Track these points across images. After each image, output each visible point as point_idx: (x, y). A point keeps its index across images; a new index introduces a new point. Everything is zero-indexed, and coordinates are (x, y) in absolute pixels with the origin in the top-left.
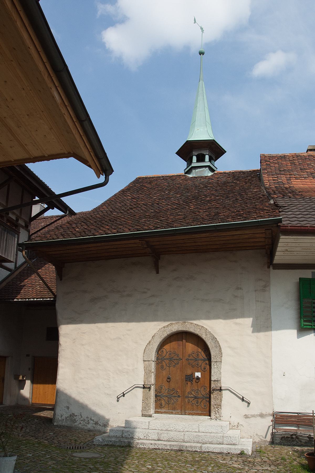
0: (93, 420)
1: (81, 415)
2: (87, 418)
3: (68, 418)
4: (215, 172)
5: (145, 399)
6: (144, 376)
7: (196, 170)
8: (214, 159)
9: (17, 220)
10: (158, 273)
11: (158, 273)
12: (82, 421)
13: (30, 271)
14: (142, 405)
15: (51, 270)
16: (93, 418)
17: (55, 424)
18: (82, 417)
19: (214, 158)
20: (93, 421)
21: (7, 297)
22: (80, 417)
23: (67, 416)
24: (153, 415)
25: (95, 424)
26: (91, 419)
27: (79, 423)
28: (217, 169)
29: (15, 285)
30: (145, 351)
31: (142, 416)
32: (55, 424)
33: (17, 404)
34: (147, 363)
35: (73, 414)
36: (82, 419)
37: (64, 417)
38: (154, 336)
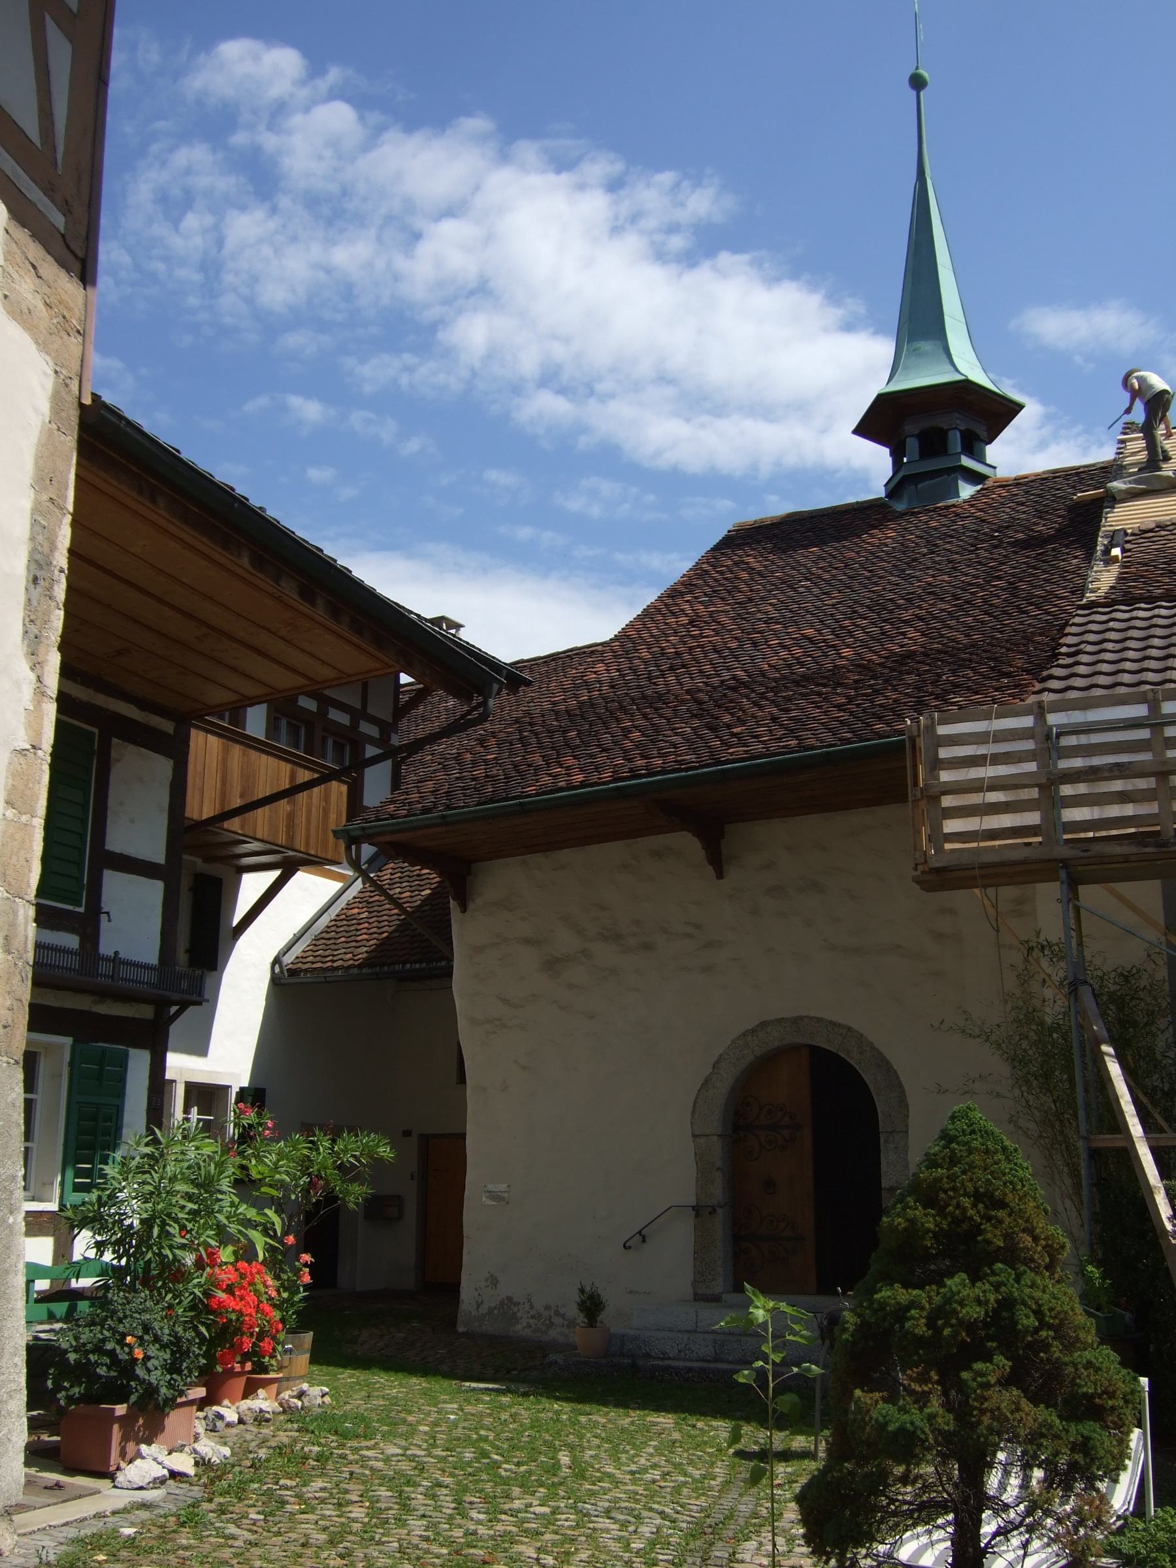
0: (563, 1316)
1: (529, 1301)
2: (547, 1308)
3: (496, 1312)
4: (989, 483)
5: (701, 1250)
6: (697, 1179)
7: (919, 486)
8: (982, 437)
9: (354, 725)
10: (720, 875)
11: (720, 875)
12: (533, 1317)
13: (399, 875)
14: (695, 1266)
15: (384, 913)
16: (562, 1311)
17: (461, 1329)
18: (532, 1307)
19: (983, 434)
20: (564, 1319)
21: (329, 964)
22: (527, 1306)
23: (493, 1305)
24: (724, 1297)
25: (568, 1327)
26: (557, 1314)
27: (525, 1324)
28: (995, 468)
29: (355, 921)
30: (694, 1106)
31: (695, 1299)
32: (461, 1329)
33: (800, 1521)
34: (702, 1141)
35: (510, 1299)
36: (532, 1312)
37: (484, 1309)
38: (717, 1062)
